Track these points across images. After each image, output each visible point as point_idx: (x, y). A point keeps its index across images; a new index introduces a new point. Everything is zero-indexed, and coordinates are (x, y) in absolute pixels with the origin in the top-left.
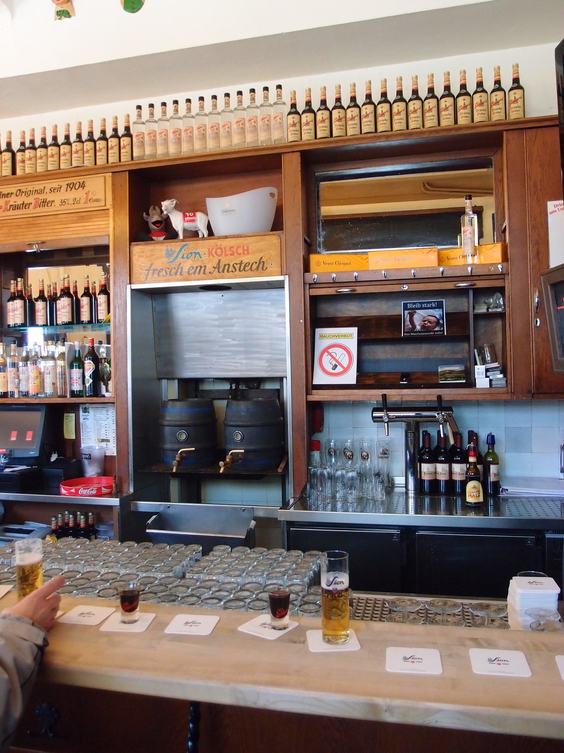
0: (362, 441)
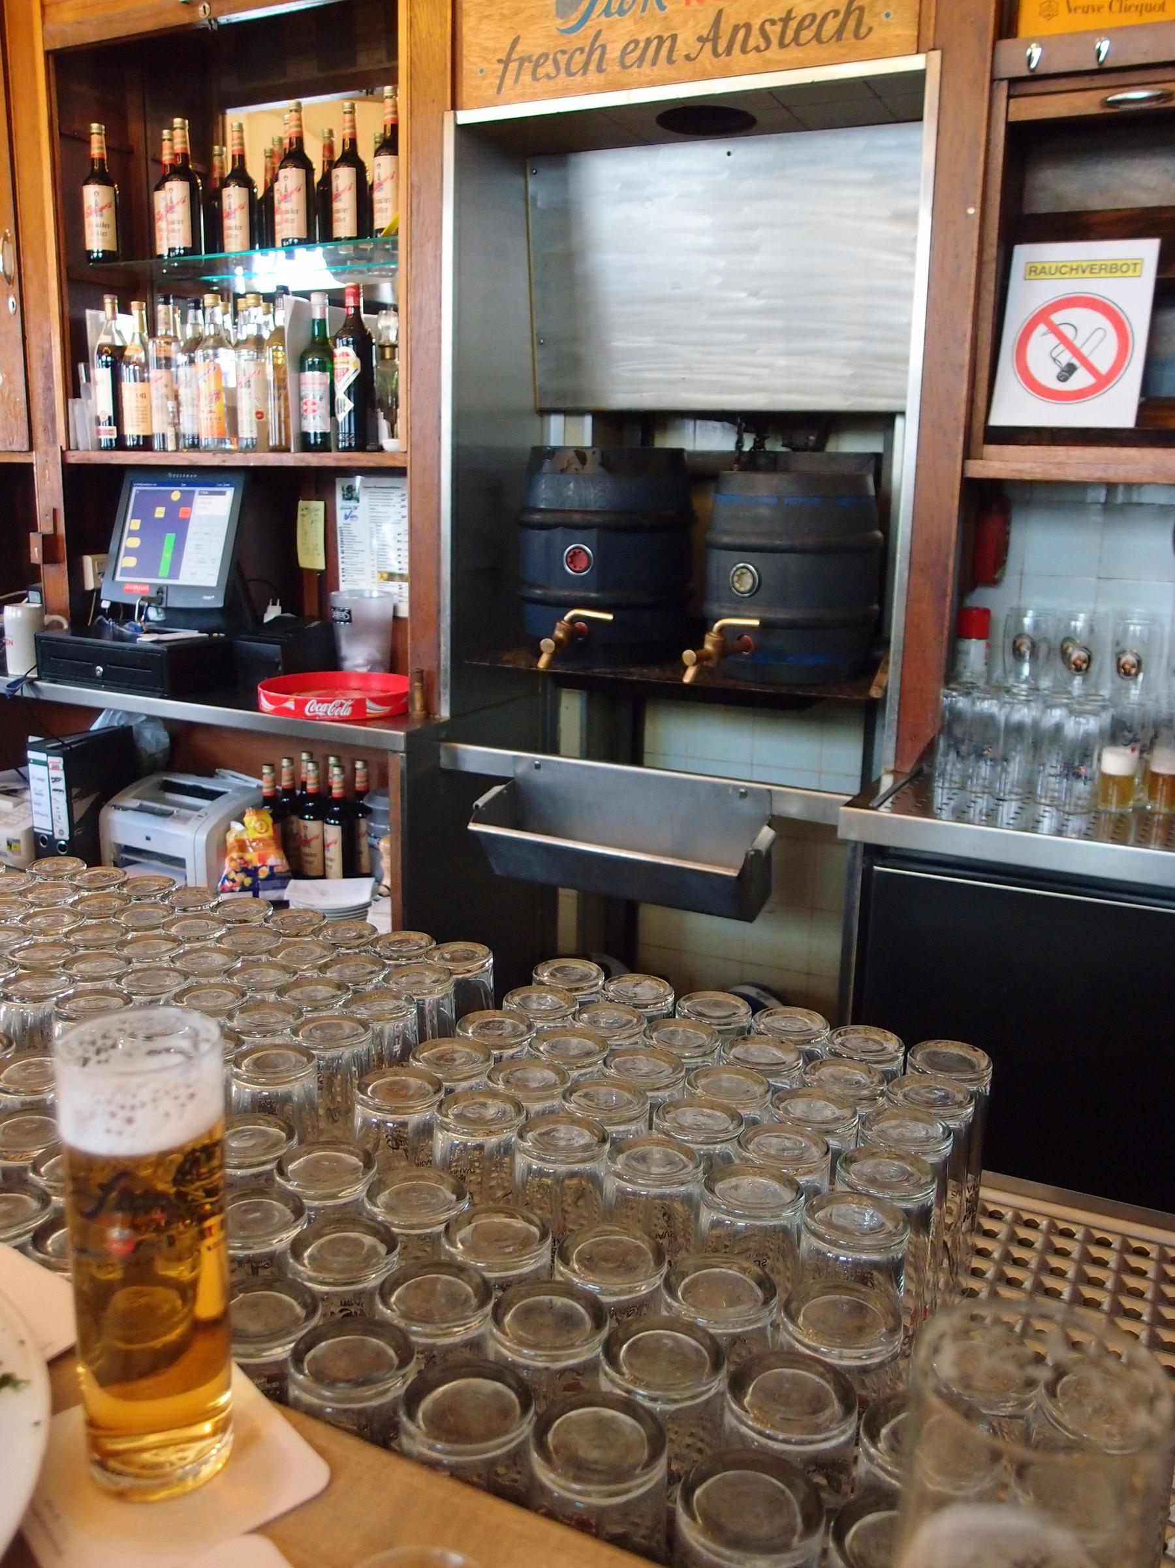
0: (1123, 619)
